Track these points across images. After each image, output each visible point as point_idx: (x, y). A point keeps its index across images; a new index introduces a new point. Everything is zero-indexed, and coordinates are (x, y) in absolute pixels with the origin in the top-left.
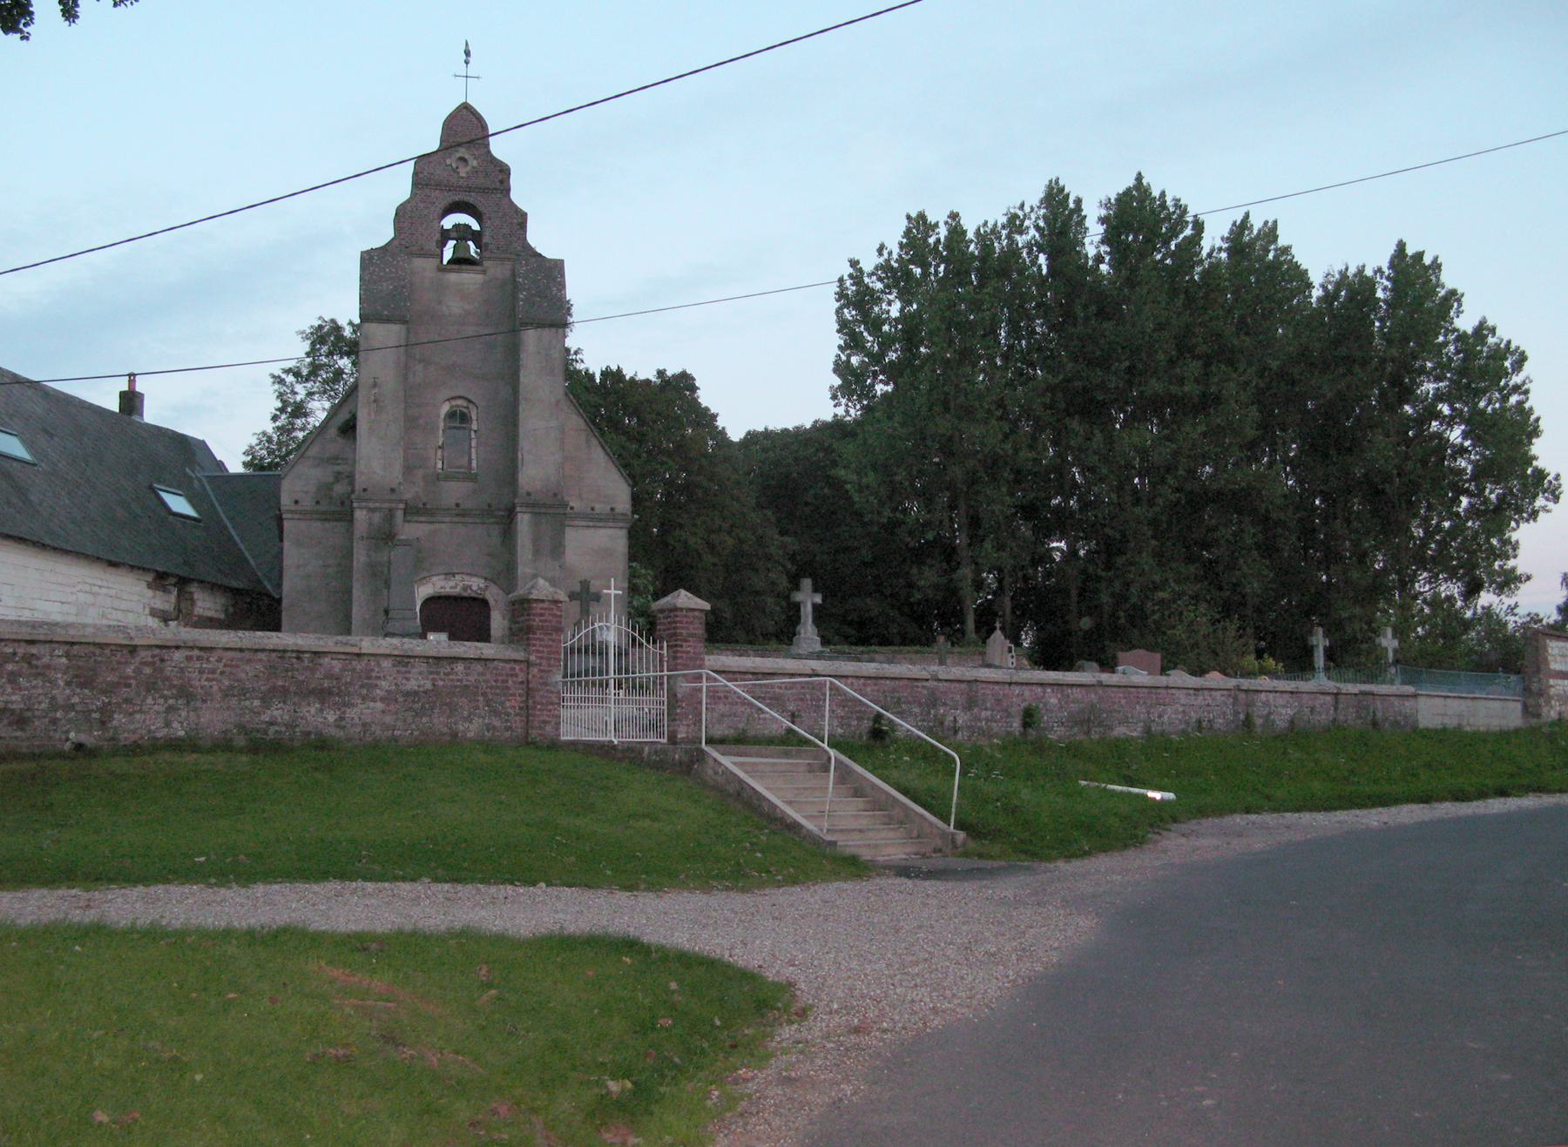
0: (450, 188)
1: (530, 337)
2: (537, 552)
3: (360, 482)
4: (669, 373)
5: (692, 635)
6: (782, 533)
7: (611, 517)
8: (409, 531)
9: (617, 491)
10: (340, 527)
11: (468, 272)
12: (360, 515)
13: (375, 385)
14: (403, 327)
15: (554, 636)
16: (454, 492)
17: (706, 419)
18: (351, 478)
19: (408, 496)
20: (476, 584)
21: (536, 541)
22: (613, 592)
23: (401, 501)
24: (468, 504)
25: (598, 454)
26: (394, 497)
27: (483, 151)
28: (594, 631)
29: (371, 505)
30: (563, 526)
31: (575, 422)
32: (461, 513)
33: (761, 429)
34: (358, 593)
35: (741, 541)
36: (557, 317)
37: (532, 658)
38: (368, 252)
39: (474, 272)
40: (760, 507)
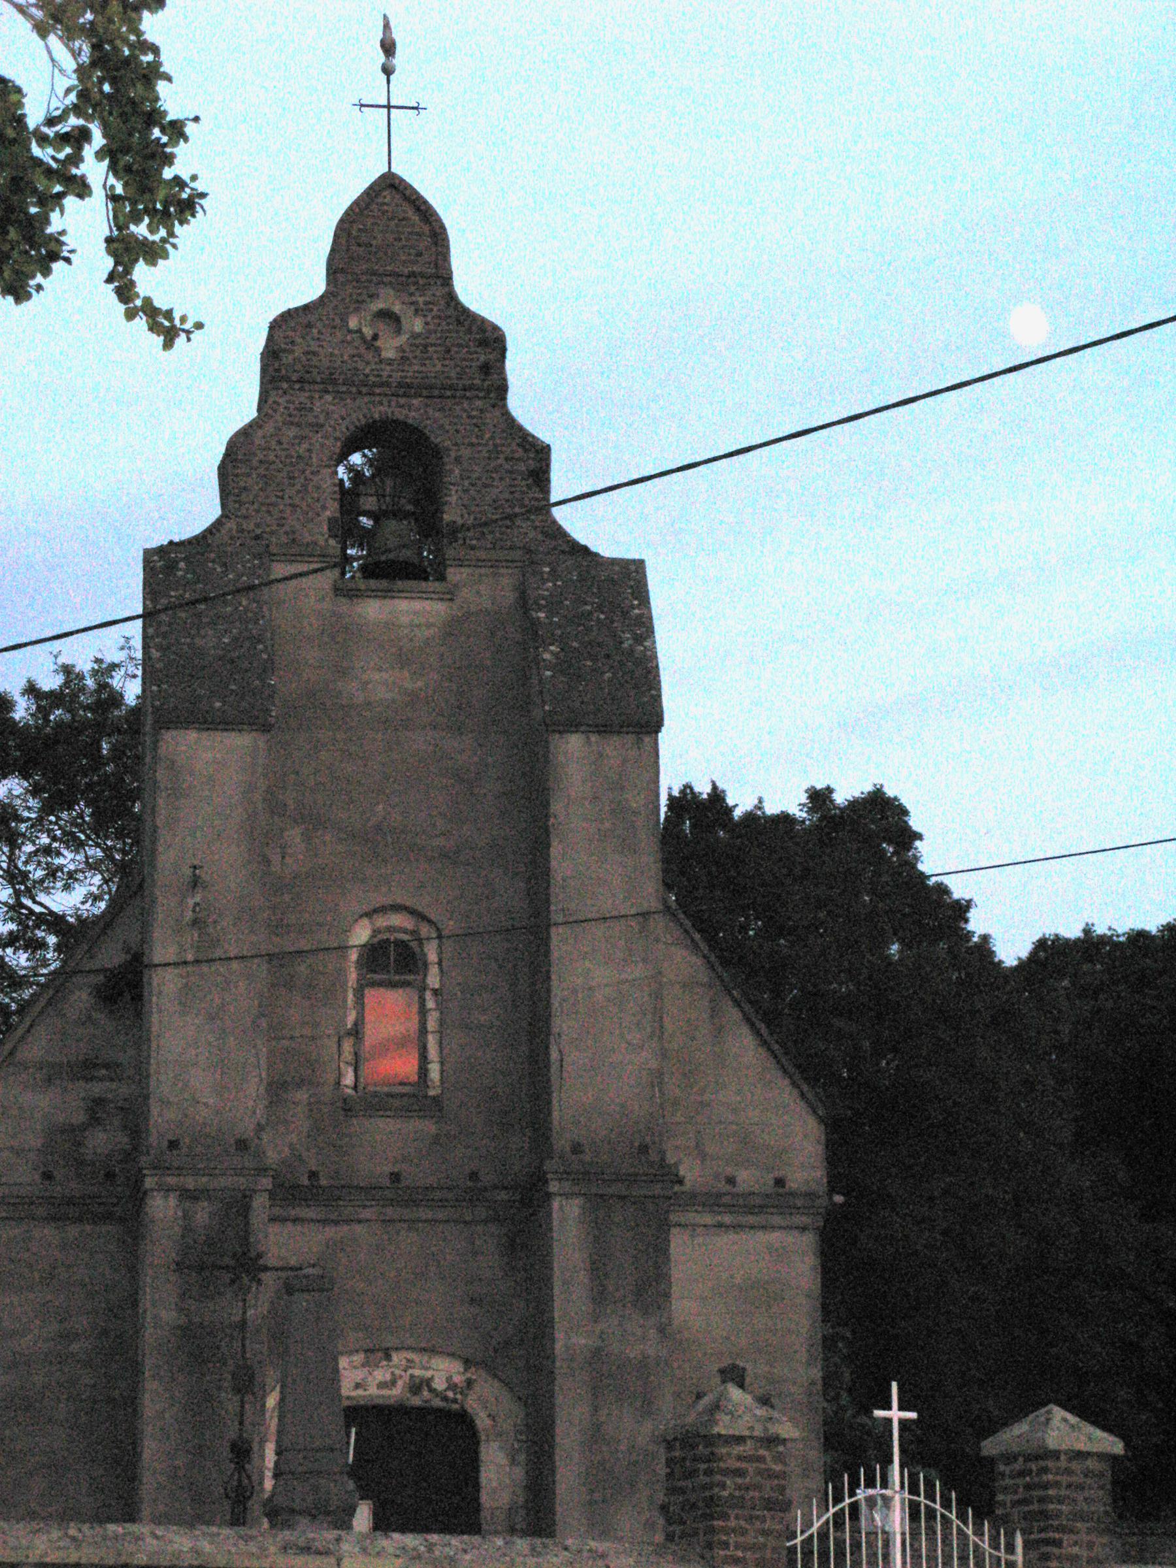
0: (364, 387)
2: (600, 1296)
3: (161, 1120)
4: (841, 797)
5: (1081, 1516)
7: (777, 1201)
8: (283, 1242)
9: (790, 1136)
12: (162, 1208)
14: (261, 740)
16: (384, 1145)
17: (942, 913)
20: (443, 1372)
21: (597, 1269)
22: (895, 1414)
23: (262, 1171)
25: (744, 1047)
28: (854, 1507)
29: (190, 1183)
30: (664, 1227)
32: (398, 1193)
33: (1072, 931)
34: (157, 1402)
36: (635, 711)
38: (161, 551)
39: (424, 595)
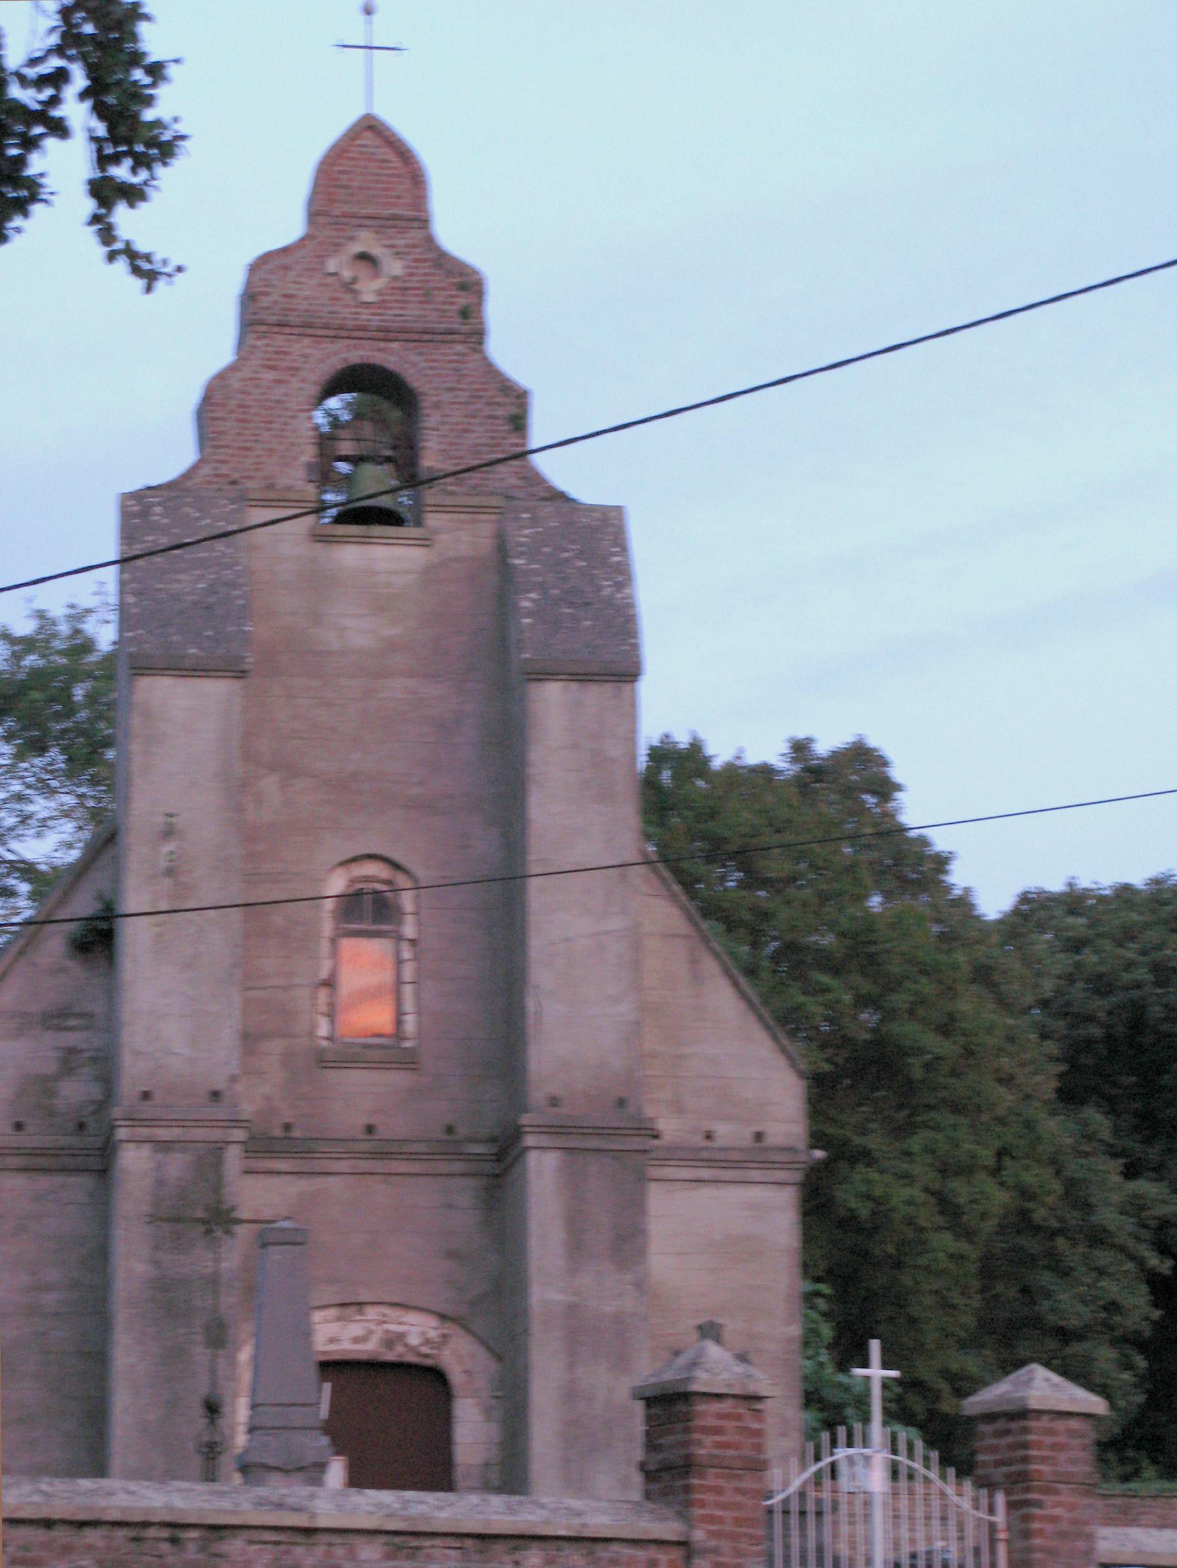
1: (551, 702)
2: (576, 1249)
3: (133, 1073)
4: (822, 748)
5: (1066, 1478)
6: (1131, 1172)
8: (258, 1195)
9: (761, 1085)
10: (84, 1182)
11: (388, 541)
12: (134, 1160)
13: (168, 833)
15: (749, 1483)
17: (915, 867)
18: (105, 1065)
19: (247, 1110)
20: (417, 1332)
21: (575, 1222)
23: (235, 1123)
24: (394, 1127)
25: (723, 1000)
26: (220, 1112)
27: (416, 235)
29: (163, 1134)
30: (642, 1179)
31: (660, 913)
32: (377, 1149)
34: (128, 1356)
35: (1026, 1194)
37: (698, 1535)
40: (1070, 1096)
